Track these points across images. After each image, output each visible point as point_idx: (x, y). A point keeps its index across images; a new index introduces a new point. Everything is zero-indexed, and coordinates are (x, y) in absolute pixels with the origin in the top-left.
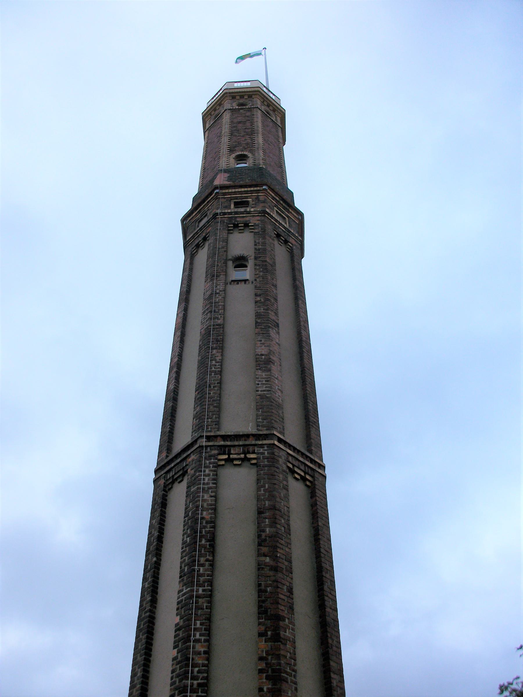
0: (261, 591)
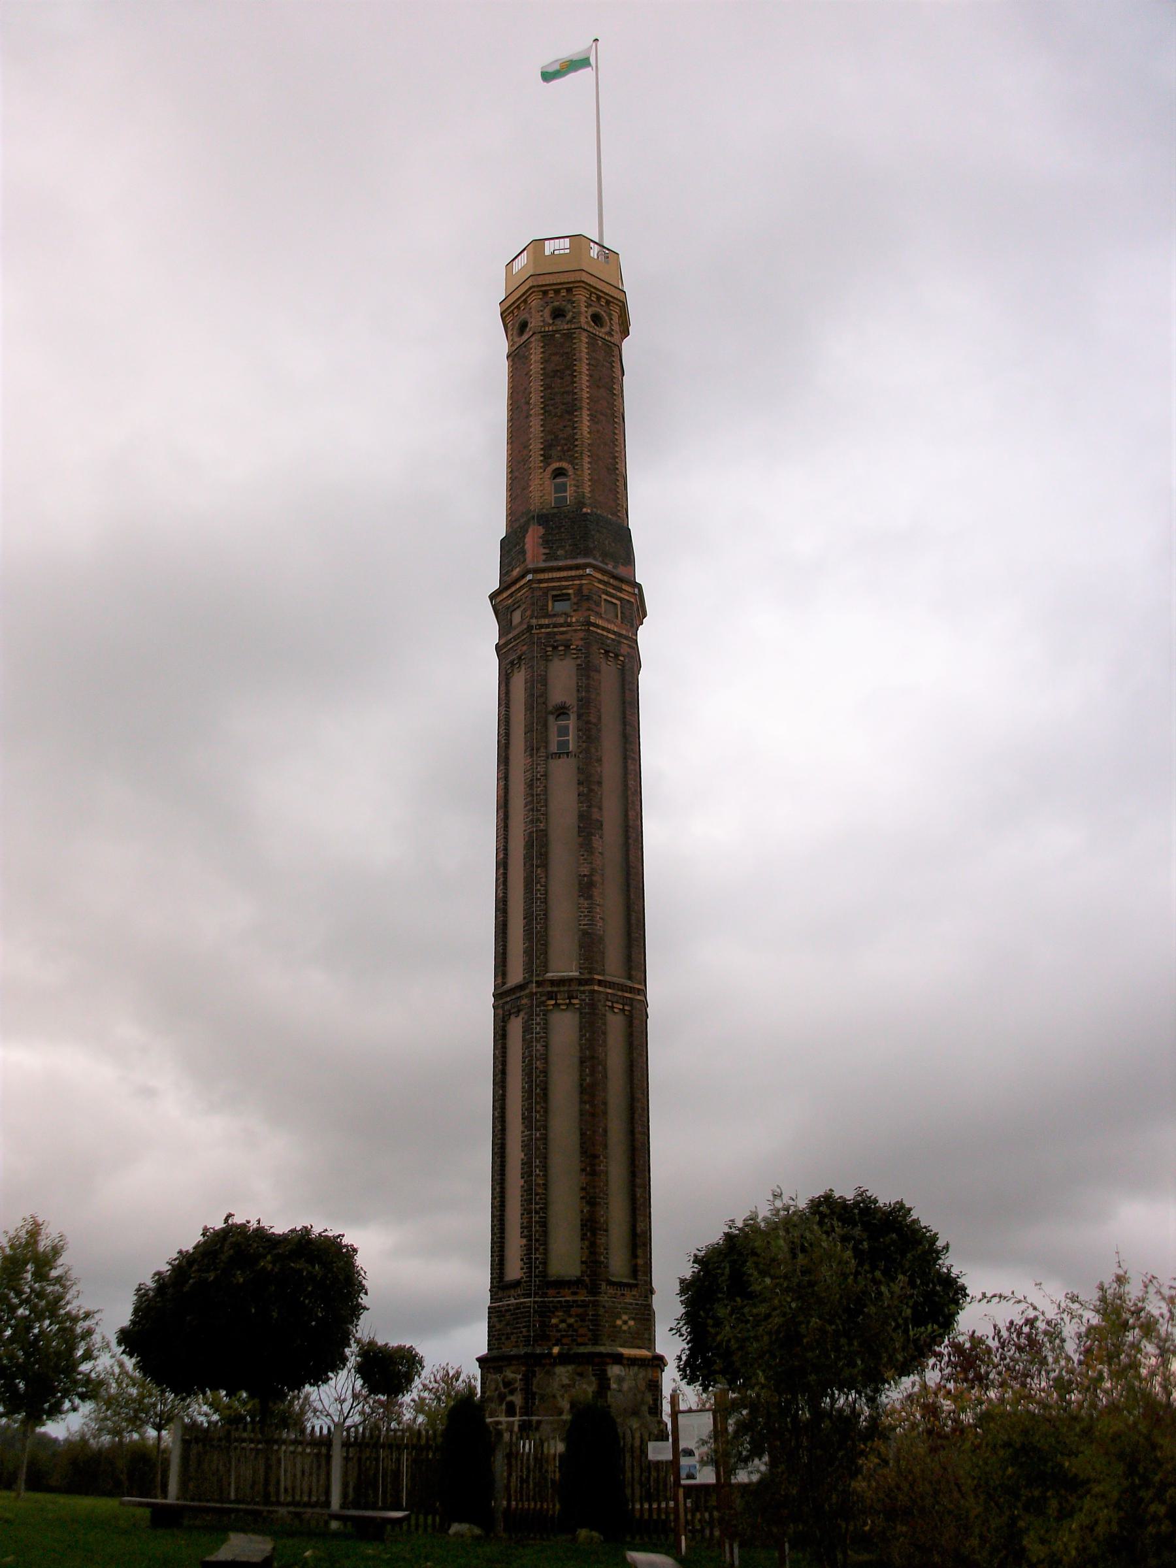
0: (583, 1134)
